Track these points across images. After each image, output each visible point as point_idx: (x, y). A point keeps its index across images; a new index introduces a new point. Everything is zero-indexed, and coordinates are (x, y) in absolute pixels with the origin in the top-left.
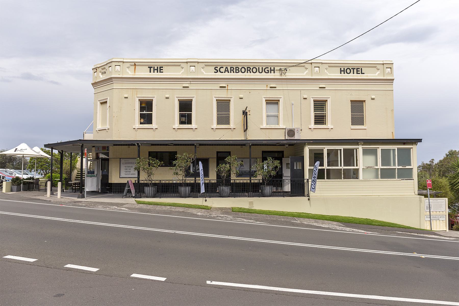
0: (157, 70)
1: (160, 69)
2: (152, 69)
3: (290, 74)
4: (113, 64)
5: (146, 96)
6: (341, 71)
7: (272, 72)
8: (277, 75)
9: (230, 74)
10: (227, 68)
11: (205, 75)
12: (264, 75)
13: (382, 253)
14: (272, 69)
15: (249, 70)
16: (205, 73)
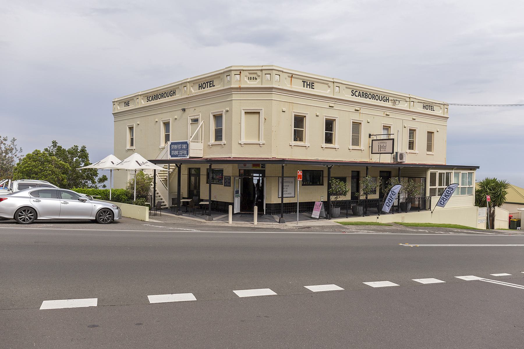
0: (310, 85)
1: (311, 85)
2: (305, 83)
3: (399, 106)
4: (275, 72)
5: (300, 111)
6: (199, 87)
8: (389, 104)
11: (249, 84)
12: (170, 99)
13: (452, 251)
15: (373, 97)
16: (248, 82)
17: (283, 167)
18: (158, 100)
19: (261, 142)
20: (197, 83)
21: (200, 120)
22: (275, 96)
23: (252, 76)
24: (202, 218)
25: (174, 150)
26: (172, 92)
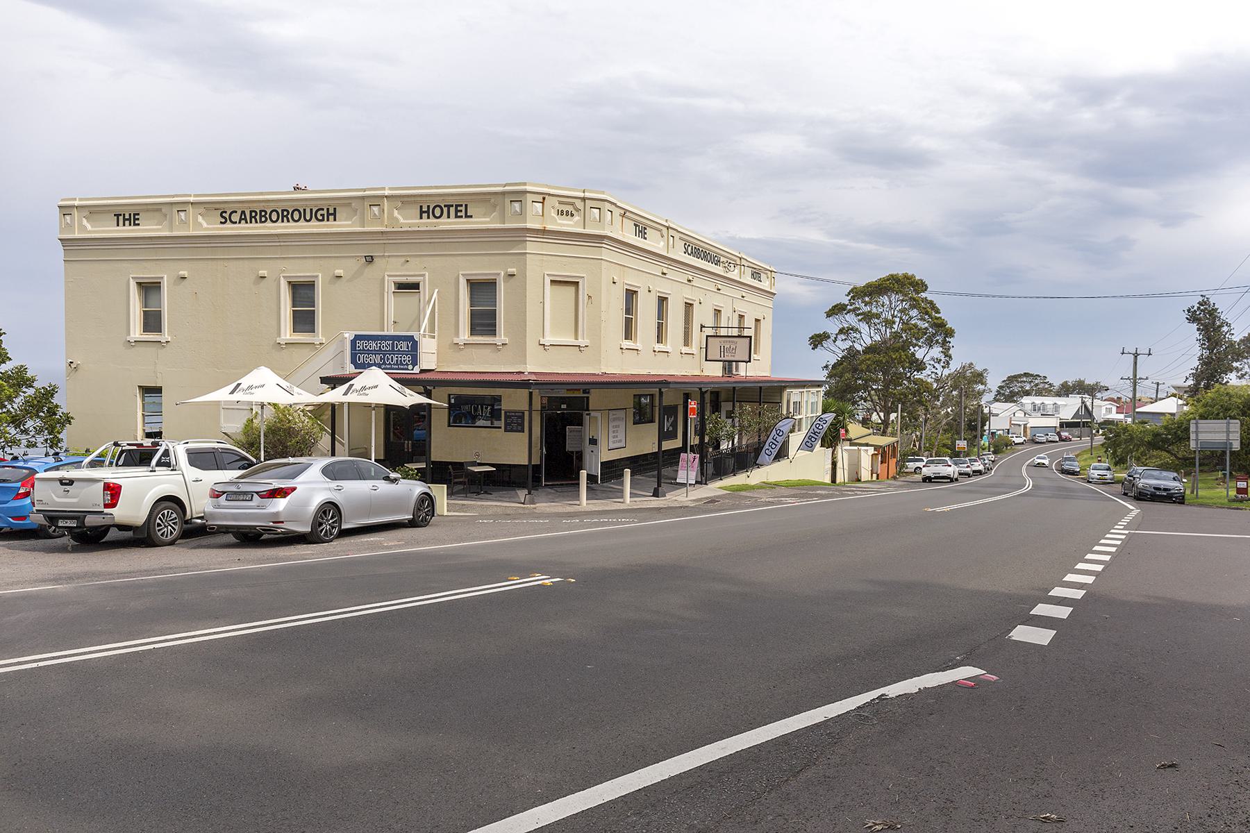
0: (129, 220)
2: (121, 218)
6: (422, 212)
7: (331, 218)
9: (249, 225)
10: (243, 212)
12: (314, 227)
14: (331, 211)
15: (285, 215)
17: (531, 393)
18: (268, 224)
19: (581, 342)
20: (415, 202)
21: (425, 288)
22: (607, 253)
23: (565, 208)
24: (487, 499)
25: (363, 351)
26: (326, 211)
